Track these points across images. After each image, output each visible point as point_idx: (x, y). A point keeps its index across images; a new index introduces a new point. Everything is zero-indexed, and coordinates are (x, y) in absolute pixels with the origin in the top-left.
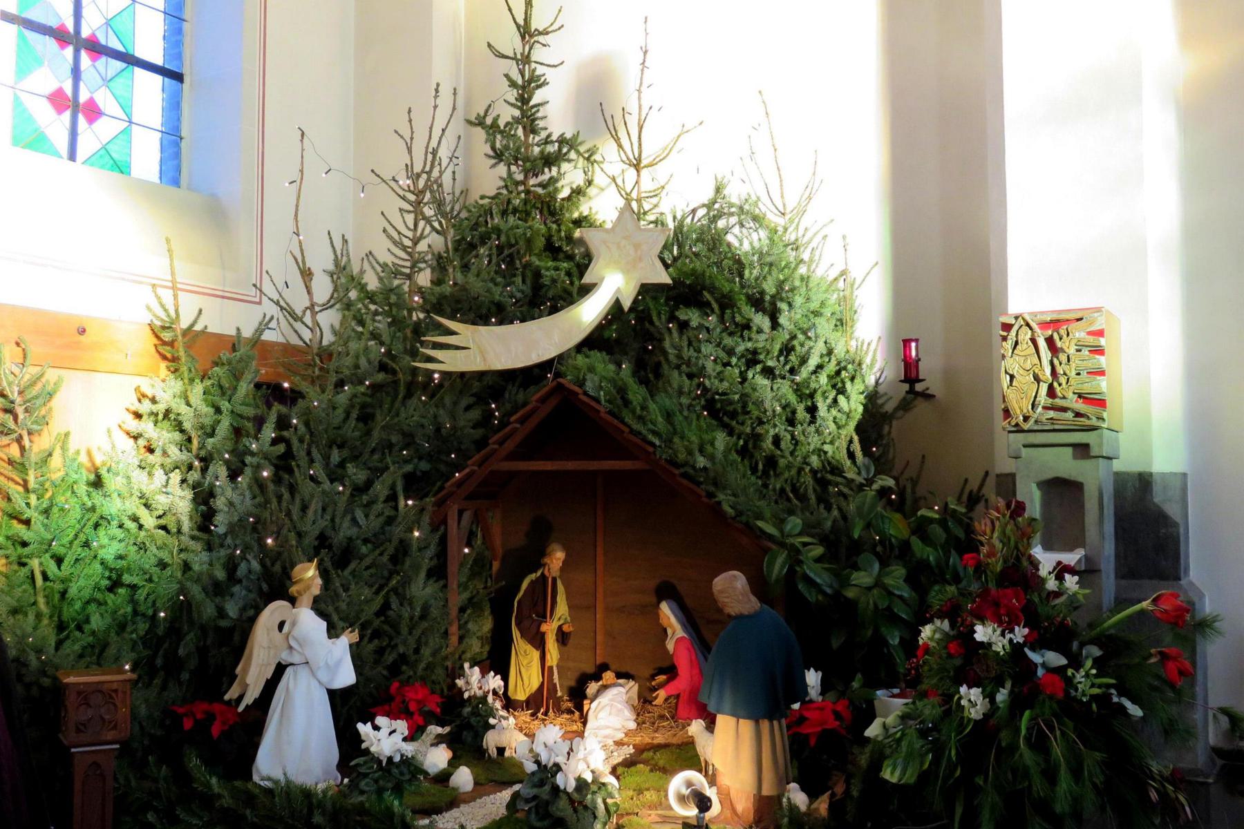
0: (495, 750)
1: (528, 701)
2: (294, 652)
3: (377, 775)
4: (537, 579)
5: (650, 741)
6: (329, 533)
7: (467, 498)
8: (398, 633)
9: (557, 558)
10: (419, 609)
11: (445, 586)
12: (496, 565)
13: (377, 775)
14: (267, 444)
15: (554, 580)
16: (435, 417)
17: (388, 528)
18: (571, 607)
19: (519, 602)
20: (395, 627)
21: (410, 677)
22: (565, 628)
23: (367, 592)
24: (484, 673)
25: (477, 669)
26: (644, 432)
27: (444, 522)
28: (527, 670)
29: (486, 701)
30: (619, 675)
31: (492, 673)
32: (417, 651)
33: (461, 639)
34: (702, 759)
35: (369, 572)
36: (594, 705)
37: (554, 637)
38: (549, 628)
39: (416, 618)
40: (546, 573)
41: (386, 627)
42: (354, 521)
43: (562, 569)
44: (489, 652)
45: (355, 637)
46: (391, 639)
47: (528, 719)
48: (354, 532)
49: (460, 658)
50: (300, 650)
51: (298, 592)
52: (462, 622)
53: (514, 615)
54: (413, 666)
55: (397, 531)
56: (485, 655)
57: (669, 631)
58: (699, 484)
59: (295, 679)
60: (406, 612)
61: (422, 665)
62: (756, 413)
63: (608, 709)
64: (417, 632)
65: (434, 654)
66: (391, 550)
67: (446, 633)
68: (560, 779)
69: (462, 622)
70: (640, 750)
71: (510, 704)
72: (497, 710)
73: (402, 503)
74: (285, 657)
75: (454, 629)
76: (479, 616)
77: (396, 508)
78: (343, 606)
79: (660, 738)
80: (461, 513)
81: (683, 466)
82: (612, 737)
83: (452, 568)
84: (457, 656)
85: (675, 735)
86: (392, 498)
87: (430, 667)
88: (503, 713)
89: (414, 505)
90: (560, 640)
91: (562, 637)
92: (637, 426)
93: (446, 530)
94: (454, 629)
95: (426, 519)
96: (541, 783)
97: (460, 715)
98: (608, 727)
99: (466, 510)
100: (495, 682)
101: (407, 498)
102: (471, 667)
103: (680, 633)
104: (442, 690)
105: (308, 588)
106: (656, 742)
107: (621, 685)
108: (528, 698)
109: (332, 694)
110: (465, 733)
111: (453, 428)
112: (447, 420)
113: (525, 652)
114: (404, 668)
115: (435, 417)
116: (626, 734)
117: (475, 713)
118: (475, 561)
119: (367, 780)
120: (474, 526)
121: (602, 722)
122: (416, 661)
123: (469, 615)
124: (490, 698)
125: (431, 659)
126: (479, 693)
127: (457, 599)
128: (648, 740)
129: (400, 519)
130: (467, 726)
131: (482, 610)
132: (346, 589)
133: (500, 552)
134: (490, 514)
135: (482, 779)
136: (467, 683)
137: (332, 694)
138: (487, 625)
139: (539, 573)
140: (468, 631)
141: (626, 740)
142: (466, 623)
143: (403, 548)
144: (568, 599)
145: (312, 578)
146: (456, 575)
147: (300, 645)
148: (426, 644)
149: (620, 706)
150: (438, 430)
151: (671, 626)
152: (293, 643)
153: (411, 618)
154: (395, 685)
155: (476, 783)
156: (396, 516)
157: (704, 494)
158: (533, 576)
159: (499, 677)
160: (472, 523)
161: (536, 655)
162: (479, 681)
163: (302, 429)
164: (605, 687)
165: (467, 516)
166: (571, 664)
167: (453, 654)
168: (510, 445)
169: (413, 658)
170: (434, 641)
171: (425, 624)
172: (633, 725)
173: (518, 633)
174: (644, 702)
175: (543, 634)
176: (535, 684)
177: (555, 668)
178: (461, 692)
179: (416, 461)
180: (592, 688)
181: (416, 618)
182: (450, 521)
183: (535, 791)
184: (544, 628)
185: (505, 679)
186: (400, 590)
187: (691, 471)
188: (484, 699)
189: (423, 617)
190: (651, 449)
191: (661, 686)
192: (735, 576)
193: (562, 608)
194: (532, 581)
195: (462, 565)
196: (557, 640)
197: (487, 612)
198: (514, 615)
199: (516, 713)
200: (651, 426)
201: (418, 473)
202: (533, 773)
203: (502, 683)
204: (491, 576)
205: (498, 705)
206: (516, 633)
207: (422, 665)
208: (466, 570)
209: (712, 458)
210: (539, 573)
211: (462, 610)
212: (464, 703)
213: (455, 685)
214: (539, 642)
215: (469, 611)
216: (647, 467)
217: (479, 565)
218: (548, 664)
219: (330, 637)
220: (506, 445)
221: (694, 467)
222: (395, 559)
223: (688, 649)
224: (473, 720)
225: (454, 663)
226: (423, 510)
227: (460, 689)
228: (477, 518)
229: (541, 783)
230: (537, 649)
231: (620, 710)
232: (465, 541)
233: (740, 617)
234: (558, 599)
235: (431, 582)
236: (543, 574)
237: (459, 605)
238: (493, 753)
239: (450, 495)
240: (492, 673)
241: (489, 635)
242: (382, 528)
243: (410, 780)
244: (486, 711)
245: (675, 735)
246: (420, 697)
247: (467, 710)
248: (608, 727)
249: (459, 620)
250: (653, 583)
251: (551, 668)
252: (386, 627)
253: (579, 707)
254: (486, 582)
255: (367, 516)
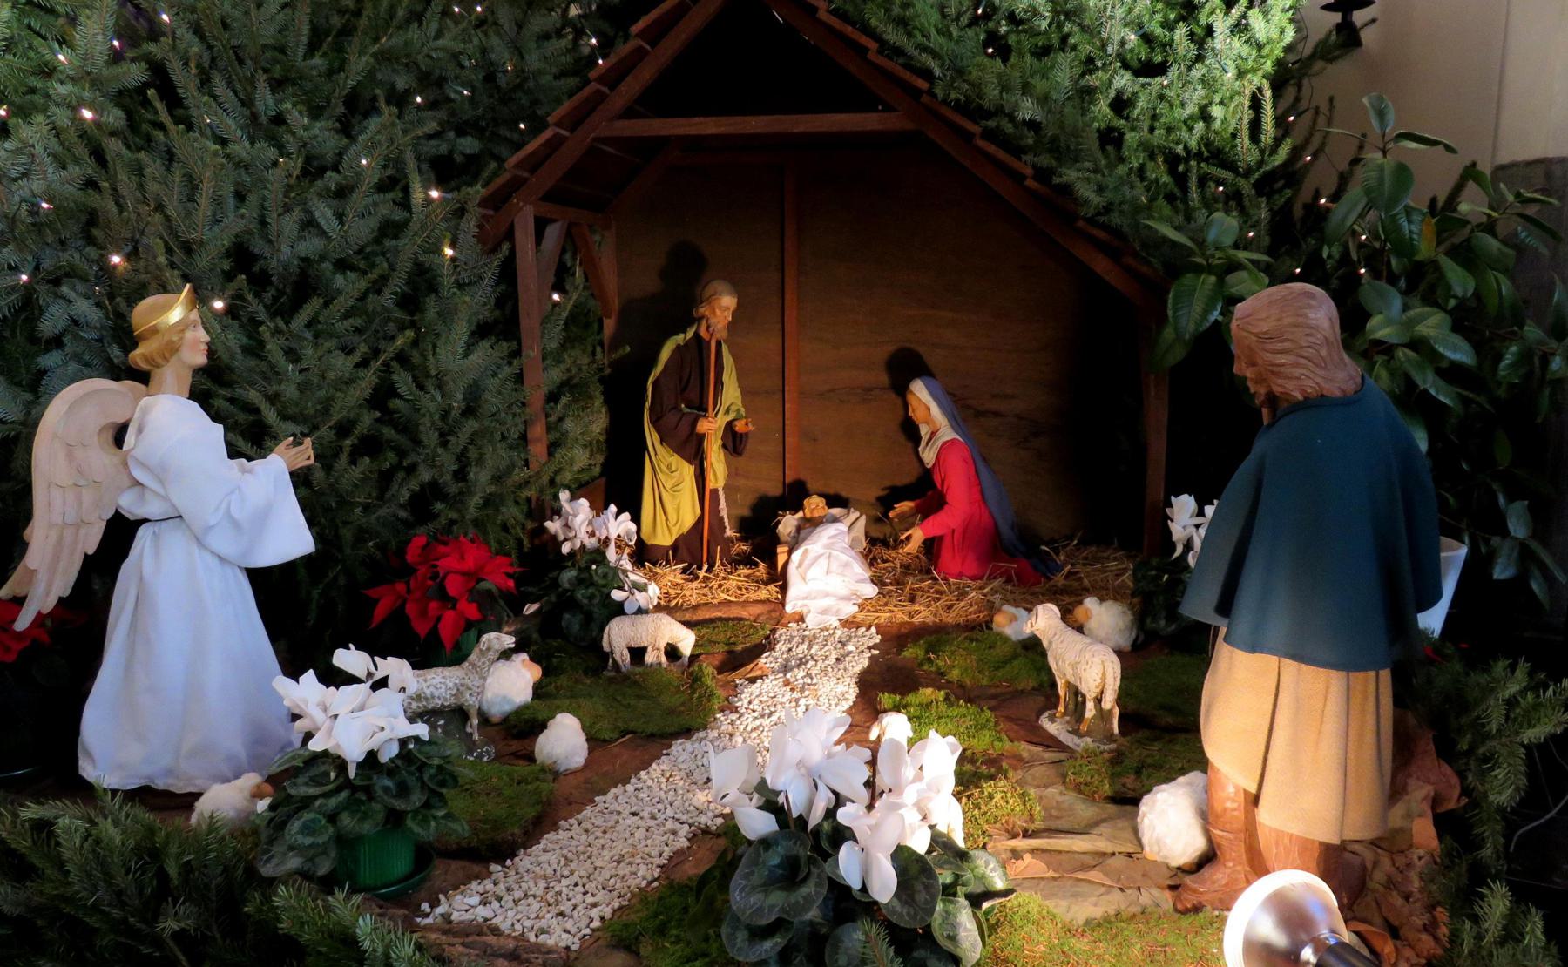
0: (626, 652)
1: (675, 547)
2: (148, 495)
3: (333, 802)
4: (687, 344)
5: (906, 619)
6: (258, 246)
7: (548, 197)
8: (417, 442)
9: (722, 306)
10: (460, 396)
11: (517, 353)
12: (609, 325)
13: (333, 802)
14: (100, 61)
15: (719, 344)
16: (484, 51)
17: (388, 243)
18: (747, 392)
19: (655, 383)
20: (408, 429)
21: (452, 522)
22: (740, 427)
23: (342, 364)
24: (599, 508)
25: (584, 502)
26: (910, 50)
27: (510, 235)
28: (674, 497)
29: (605, 557)
30: (834, 500)
31: (613, 508)
32: (461, 475)
33: (553, 447)
34: (1060, 683)
35: (348, 323)
36: (796, 556)
37: (720, 442)
38: (713, 426)
39: (455, 413)
40: (703, 333)
41: (388, 432)
42: (309, 224)
43: (731, 326)
44: (603, 465)
45: (304, 455)
46: (401, 453)
47: (679, 579)
48: (311, 246)
49: (552, 482)
50: (160, 490)
51: (146, 358)
52: (553, 419)
53: (648, 405)
54: (457, 501)
55: (407, 248)
56: (597, 470)
57: (924, 431)
58: (1018, 151)
59: (157, 554)
60: (431, 402)
61: (476, 500)
62: (1086, 49)
63: (823, 562)
64: (458, 441)
65: (497, 479)
66: (398, 283)
67: (524, 437)
68: (847, 863)
69: (553, 419)
70: (895, 639)
71: (643, 554)
72: (625, 572)
73: (417, 196)
74: (130, 505)
75: (538, 431)
76: (584, 409)
77: (405, 204)
78: (290, 391)
79: (924, 613)
80: (541, 225)
81: (989, 115)
82: (837, 612)
83: (529, 322)
84: (545, 479)
85: (950, 607)
86: (393, 183)
87: (490, 502)
88: (636, 577)
89: (442, 200)
90: (730, 445)
91: (734, 442)
92: (893, 36)
93: (513, 251)
94: (538, 431)
95: (470, 224)
96: (791, 875)
97: (555, 583)
98: (827, 595)
99: (553, 221)
100: (619, 525)
101: (426, 188)
102: (574, 498)
103: (947, 434)
104: (519, 542)
105: (172, 349)
106: (916, 620)
107: (835, 520)
108: (676, 540)
109: (260, 579)
110: (567, 616)
111: (519, 72)
112: (507, 55)
113: (669, 467)
114: (439, 506)
115: (484, 51)
116: (862, 607)
117: (584, 580)
118: (572, 319)
119: (307, 816)
120: (568, 256)
121: (812, 586)
122: (461, 493)
123: (566, 407)
124: (611, 554)
125: (493, 489)
126: (591, 543)
127: (543, 378)
128: (901, 617)
129: (414, 226)
130: (567, 602)
131: (591, 397)
132: (293, 355)
133: (616, 304)
134: (597, 238)
135: (605, 730)
136: (567, 526)
137: (260, 579)
138: (597, 422)
139: (690, 333)
140: (565, 434)
141: (861, 616)
142: (561, 419)
143: (423, 281)
144: (739, 379)
145: (182, 326)
146: (538, 338)
147: (161, 482)
148: (480, 461)
149: (844, 558)
150: (490, 78)
151: (929, 420)
152: (138, 474)
153: (445, 415)
154: (420, 537)
155: (592, 739)
156: (406, 223)
157: (1028, 171)
158: (680, 339)
159: (626, 516)
160: (563, 251)
161: (688, 471)
162: (590, 523)
163: (184, 33)
164: (812, 524)
165: (553, 232)
166: (741, 482)
167: (538, 475)
168: (631, 87)
169: (453, 489)
170: (497, 456)
171: (471, 425)
172: (871, 591)
173: (656, 437)
174: (876, 548)
175: (701, 438)
176: (688, 520)
177: (721, 493)
178: (555, 542)
179: (451, 134)
180: (787, 524)
181: (455, 413)
182: (518, 234)
183: (777, 899)
184: (703, 426)
185: (636, 519)
186: (416, 357)
187: (1009, 128)
188: (598, 555)
189: (470, 411)
190: (922, 84)
191: (907, 521)
192: (1311, 296)
193: (731, 393)
194: (678, 347)
195: (544, 321)
196: (724, 446)
197: (598, 401)
198: (648, 405)
199: (658, 570)
200: (920, 38)
201: (458, 158)
202: (766, 843)
203: (633, 527)
204: (601, 344)
205: (626, 564)
206: (651, 436)
207: (476, 500)
208: (557, 329)
209: (1044, 100)
210: (690, 333)
211: (553, 398)
212: (562, 561)
213: (545, 530)
214: (693, 451)
215: (564, 400)
216: (909, 126)
217: (580, 324)
218: (711, 483)
219: (234, 453)
220: (623, 87)
221: (1011, 118)
222: (410, 302)
223: (965, 460)
224: (580, 594)
225: (541, 491)
226: (461, 212)
227: (554, 537)
228: (571, 241)
229: (791, 875)
230: (690, 463)
231: (846, 565)
232: (551, 279)
233: (1316, 404)
234: (725, 378)
235: (485, 344)
236: (697, 335)
237: (546, 389)
238: (622, 656)
239: (515, 185)
240: (613, 508)
241: (602, 438)
242: (378, 241)
243: (427, 805)
244: (605, 576)
245: (950, 607)
246: (470, 564)
247: (568, 576)
248: (827, 595)
249: (547, 416)
250: (882, 353)
251: (715, 492)
252: (388, 432)
253: (771, 558)
254: (594, 353)
255: (340, 217)
